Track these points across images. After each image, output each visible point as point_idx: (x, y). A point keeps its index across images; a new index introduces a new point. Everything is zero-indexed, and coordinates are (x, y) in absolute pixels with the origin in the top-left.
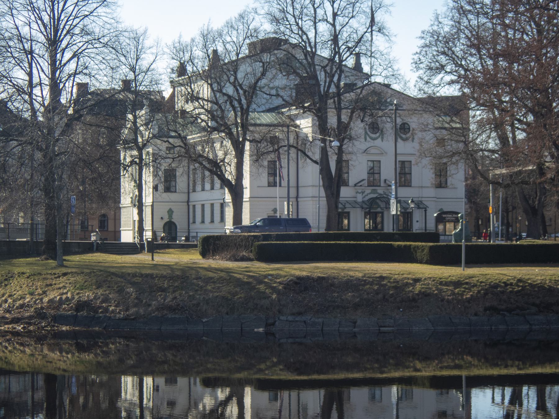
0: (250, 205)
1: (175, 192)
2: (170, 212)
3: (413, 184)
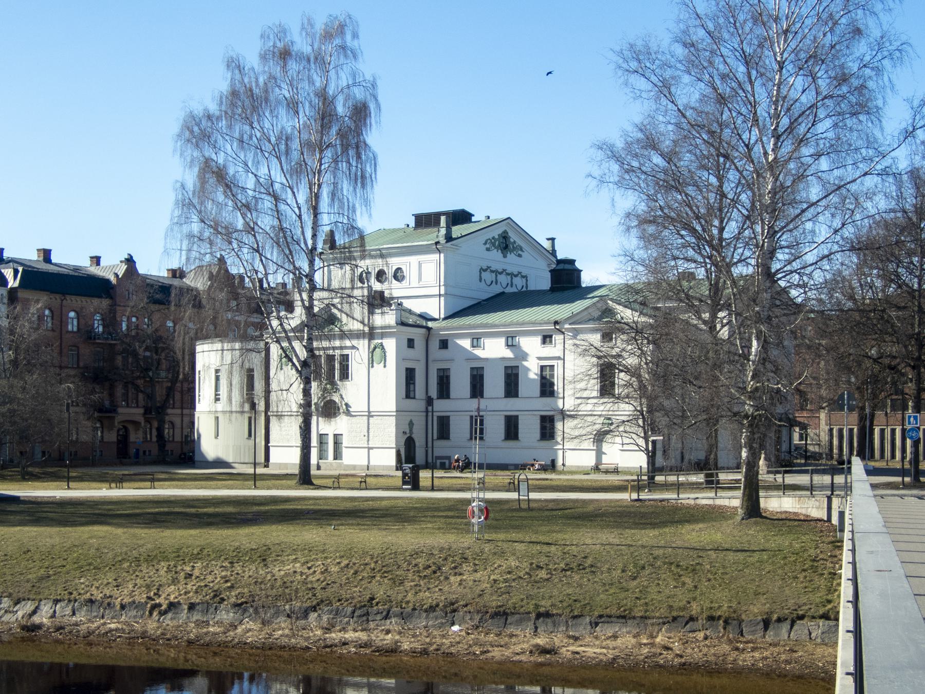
0: (396, 420)
1: (414, 398)
2: (411, 424)
3: (417, 397)
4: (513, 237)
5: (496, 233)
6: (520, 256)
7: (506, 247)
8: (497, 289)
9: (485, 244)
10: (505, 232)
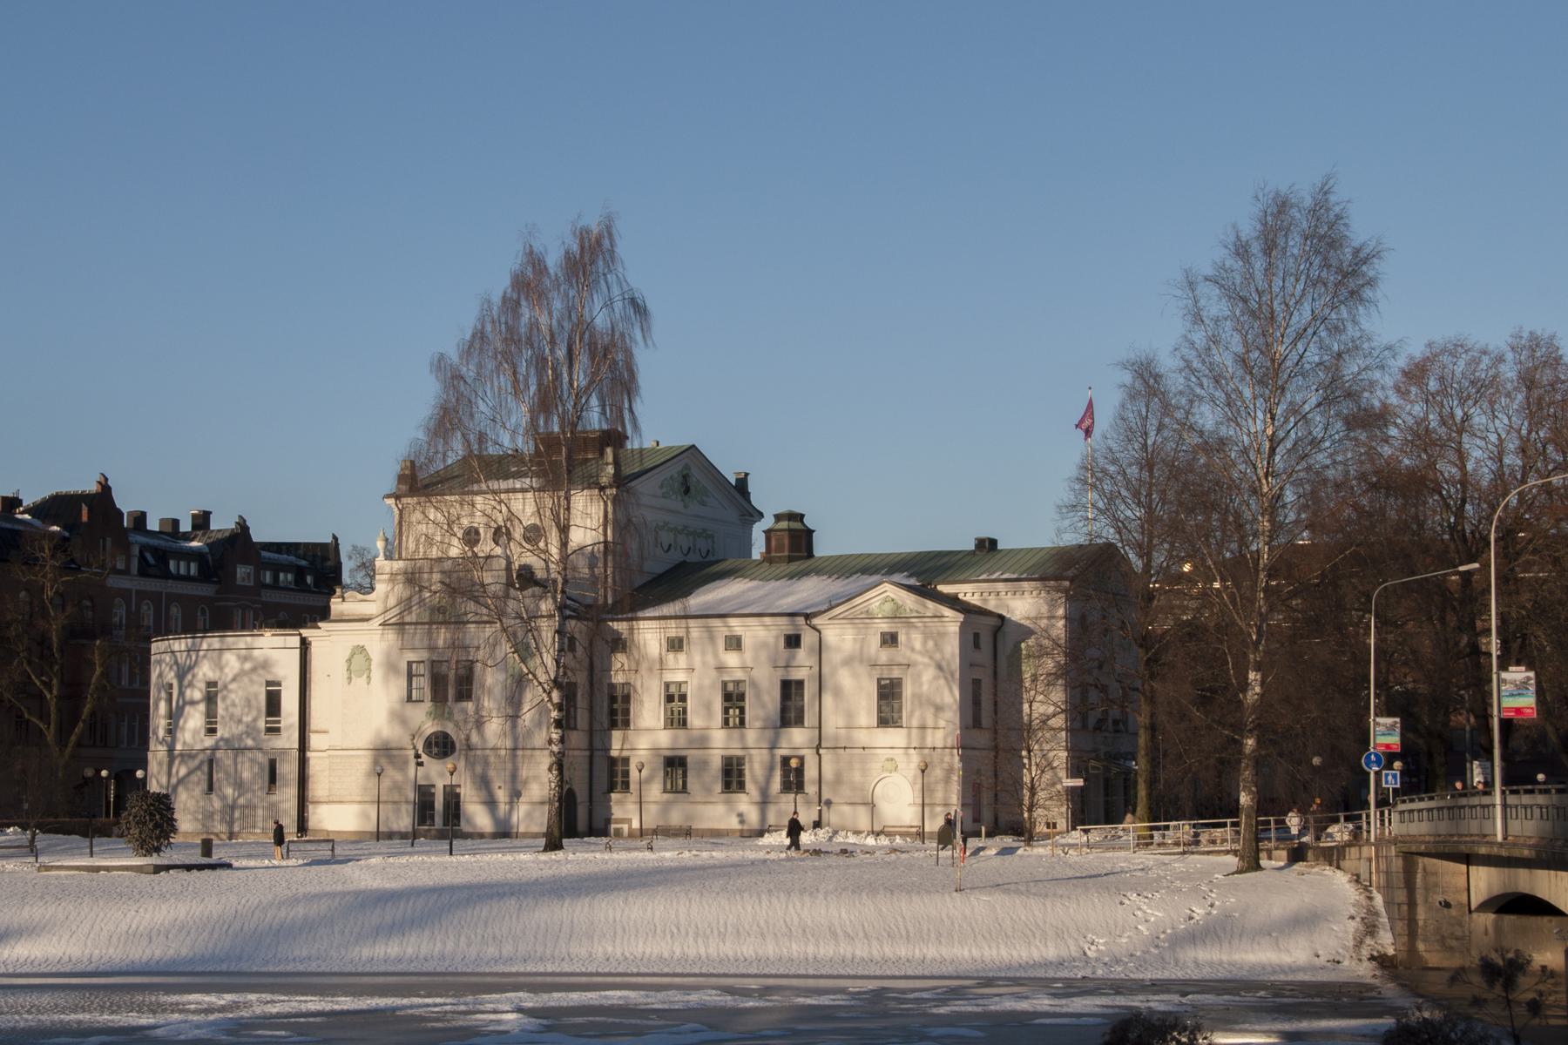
4: (696, 474)
5: (674, 470)
6: (703, 504)
7: (687, 491)
8: (676, 557)
9: (661, 487)
10: (687, 467)
